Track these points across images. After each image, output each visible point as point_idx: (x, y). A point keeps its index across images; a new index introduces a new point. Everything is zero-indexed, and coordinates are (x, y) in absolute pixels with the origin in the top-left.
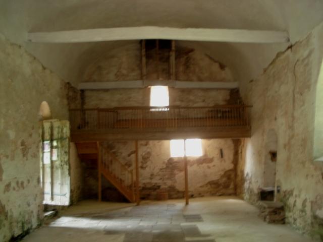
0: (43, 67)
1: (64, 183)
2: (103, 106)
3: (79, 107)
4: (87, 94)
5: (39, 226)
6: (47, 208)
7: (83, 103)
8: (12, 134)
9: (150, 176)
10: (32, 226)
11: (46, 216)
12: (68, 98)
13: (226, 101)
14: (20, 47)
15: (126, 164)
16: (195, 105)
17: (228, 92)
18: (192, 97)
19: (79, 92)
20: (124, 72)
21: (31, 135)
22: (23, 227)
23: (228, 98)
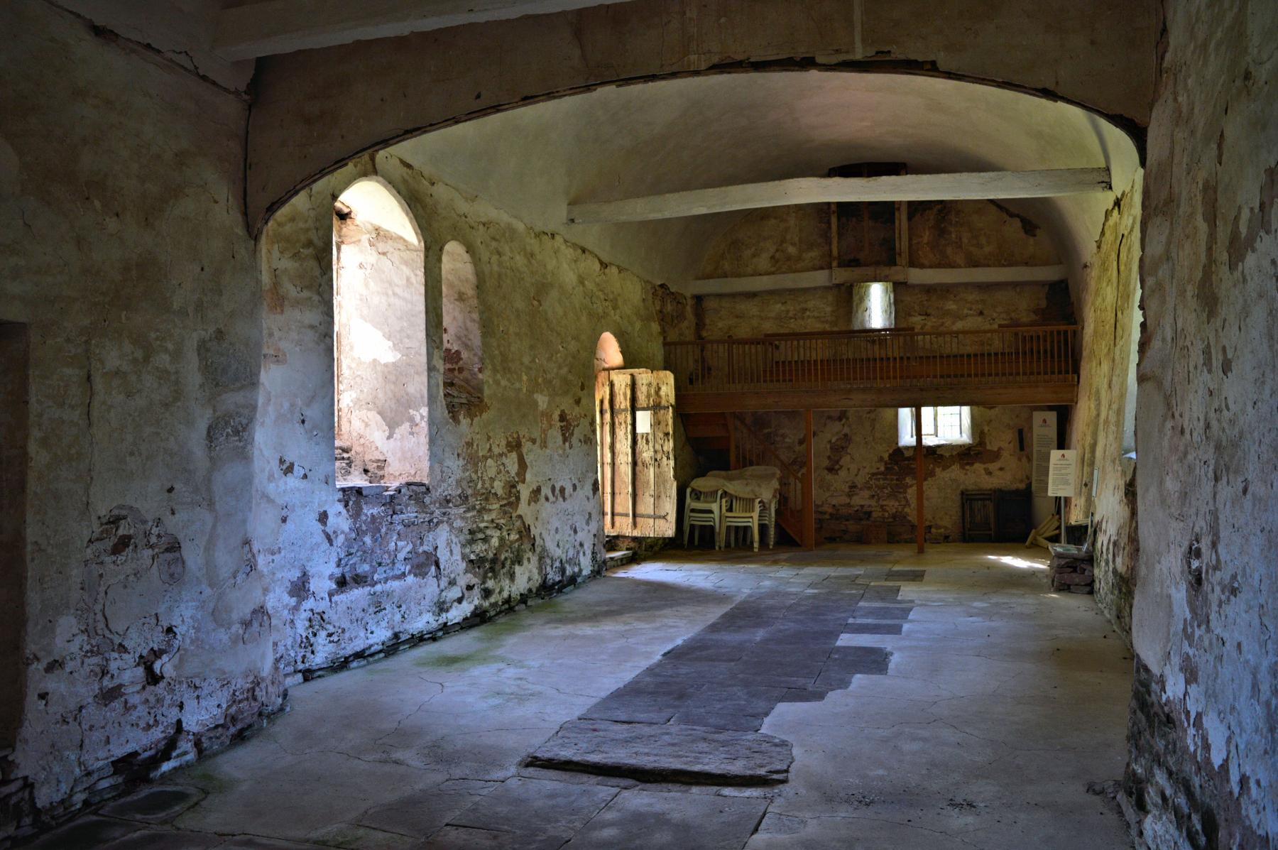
0: (601, 263)
1: (663, 496)
2: (743, 331)
3: (689, 335)
4: (710, 304)
5: (596, 574)
6: (612, 543)
7: (700, 325)
8: (542, 401)
9: (847, 490)
10: (581, 570)
11: (612, 559)
12: (663, 318)
13: (1036, 312)
14: (553, 235)
15: (794, 462)
16: (959, 325)
17: (1047, 288)
18: (951, 306)
19: (690, 302)
20: (792, 250)
21: (578, 402)
22: (563, 571)
23: (1044, 304)
